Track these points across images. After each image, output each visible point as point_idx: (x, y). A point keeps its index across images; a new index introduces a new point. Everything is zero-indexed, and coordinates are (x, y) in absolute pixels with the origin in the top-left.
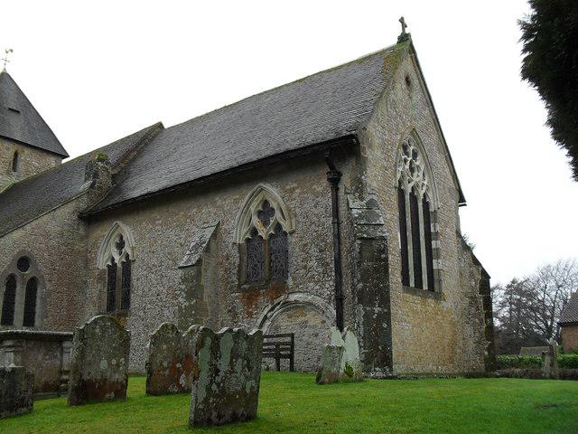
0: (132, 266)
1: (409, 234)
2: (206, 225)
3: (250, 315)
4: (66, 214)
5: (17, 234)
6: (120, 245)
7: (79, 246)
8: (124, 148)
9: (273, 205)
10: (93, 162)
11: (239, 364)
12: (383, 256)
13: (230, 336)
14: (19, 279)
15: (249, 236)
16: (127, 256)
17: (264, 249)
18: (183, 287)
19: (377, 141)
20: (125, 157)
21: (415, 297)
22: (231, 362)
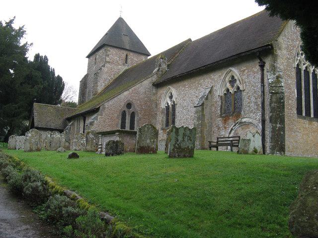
1: (303, 90)
2: (207, 88)
3: (225, 128)
5: (126, 93)
6: (171, 97)
9: (236, 78)
11: (186, 139)
13: (183, 129)
17: (232, 98)
19: (284, 46)
21: (305, 121)
22: (183, 137)
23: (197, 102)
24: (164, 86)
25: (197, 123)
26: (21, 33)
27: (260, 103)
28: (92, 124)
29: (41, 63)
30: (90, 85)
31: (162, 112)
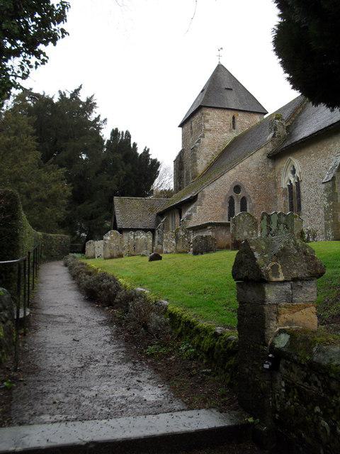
5: (231, 172)
6: (294, 172)
7: (270, 175)
8: (294, 107)
10: (278, 115)
11: (281, 227)
16: (298, 179)
20: (294, 113)
24: (296, 151)
26: (90, 105)
28: (189, 218)
29: (122, 143)
30: (188, 164)
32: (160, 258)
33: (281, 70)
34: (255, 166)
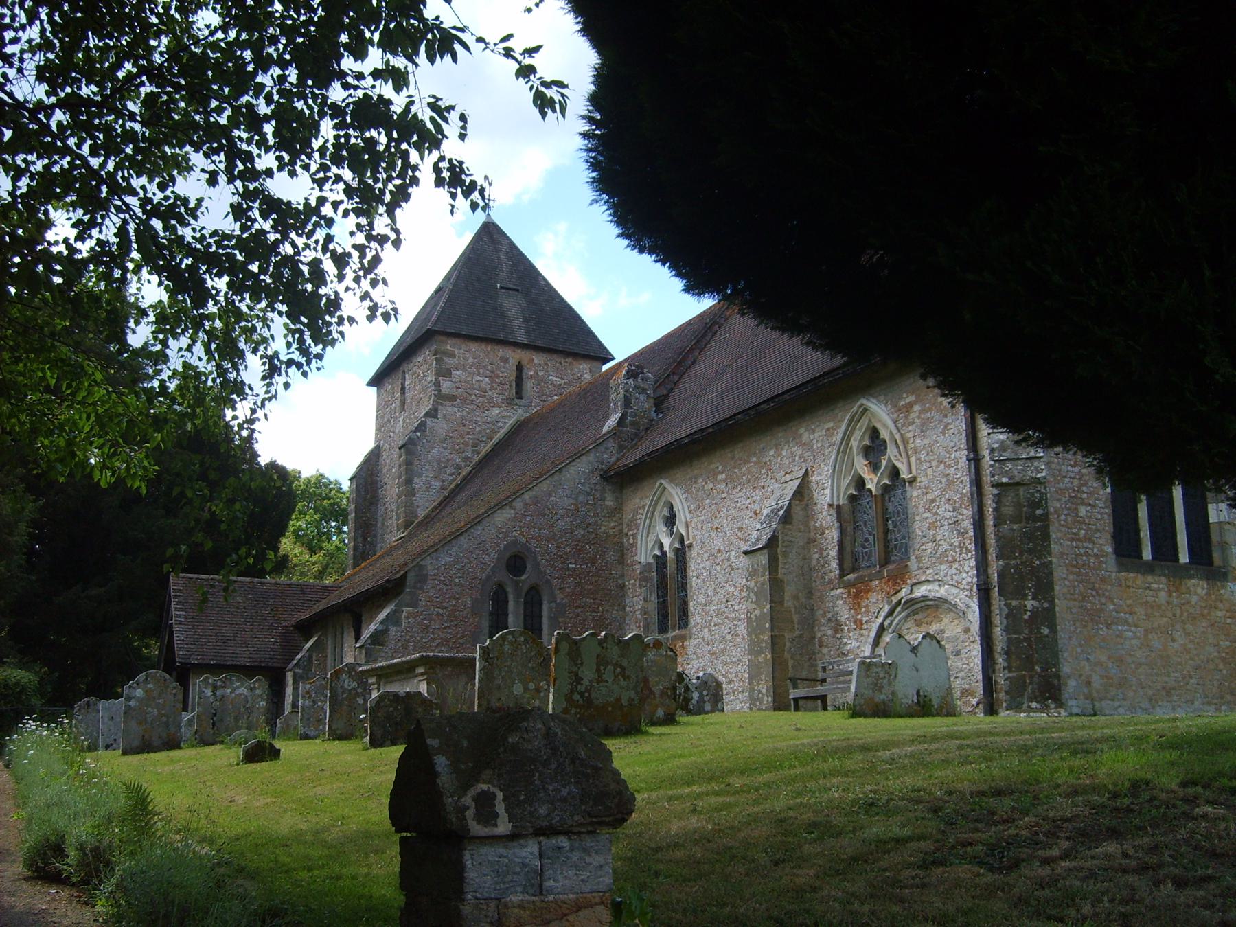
0: (688, 554)
2: (788, 477)
3: (859, 624)
4: (580, 472)
6: (671, 520)
9: (884, 434)
10: (637, 364)
11: (608, 674)
12: (1039, 512)
14: (509, 589)
15: (853, 491)
18: (752, 584)
21: (1150, 579)
22: (598, 670)
23: (755, 535)
25: (758, 612)
27: (968, 524)
30: (391, 489)
31: (644, 580)
32: (275, 754)
33: (285, 465)
34: (568, 501)
